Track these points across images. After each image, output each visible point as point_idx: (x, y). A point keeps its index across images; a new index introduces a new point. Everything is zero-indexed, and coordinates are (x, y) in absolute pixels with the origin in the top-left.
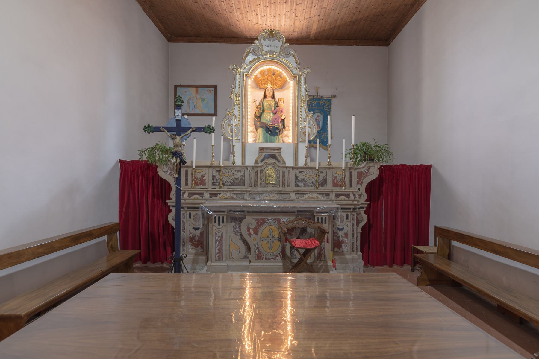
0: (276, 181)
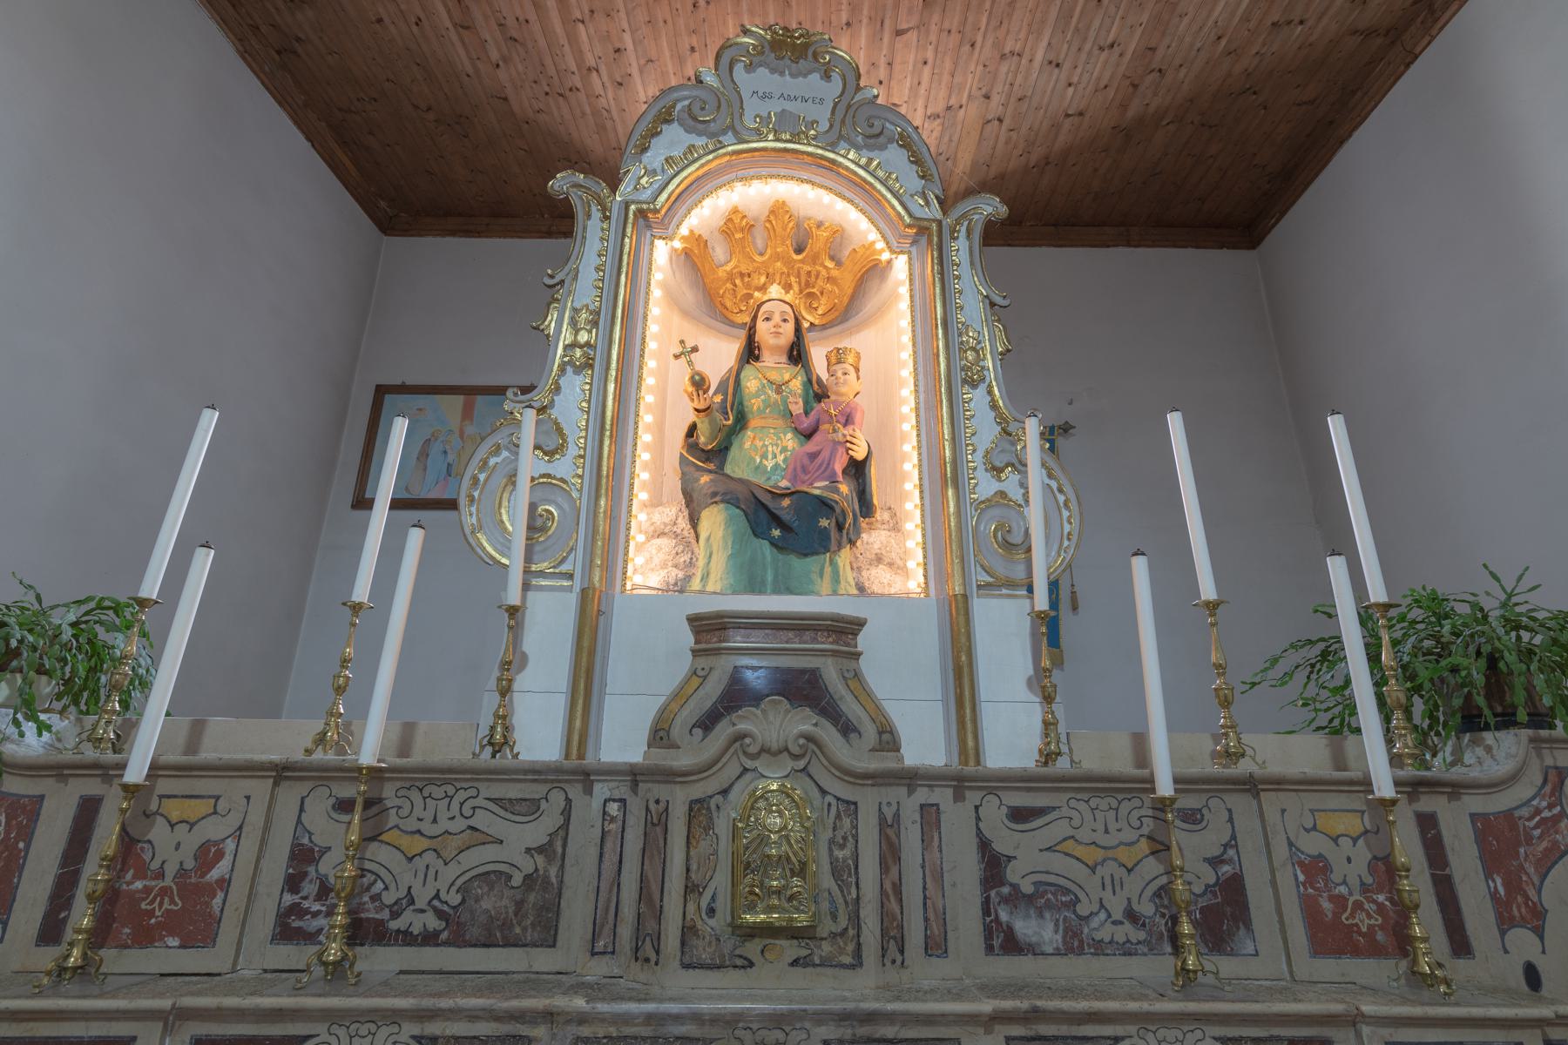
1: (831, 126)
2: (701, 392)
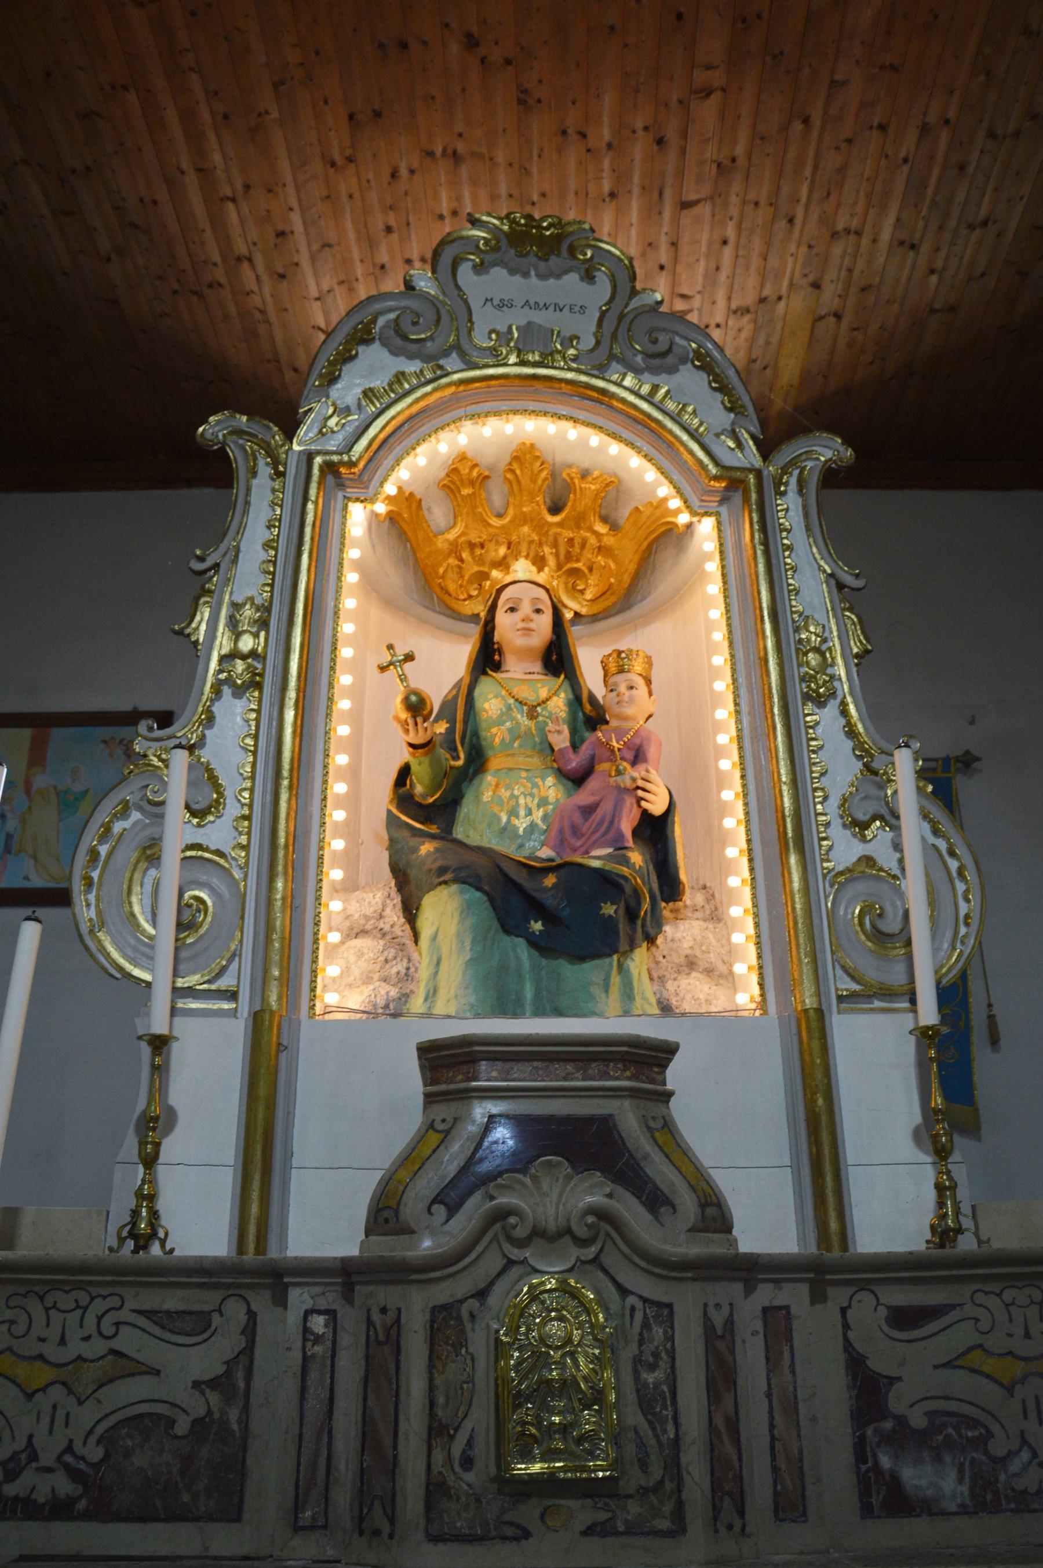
0: (630, 1450)
1: (598, 343)
2: (419, 720)
